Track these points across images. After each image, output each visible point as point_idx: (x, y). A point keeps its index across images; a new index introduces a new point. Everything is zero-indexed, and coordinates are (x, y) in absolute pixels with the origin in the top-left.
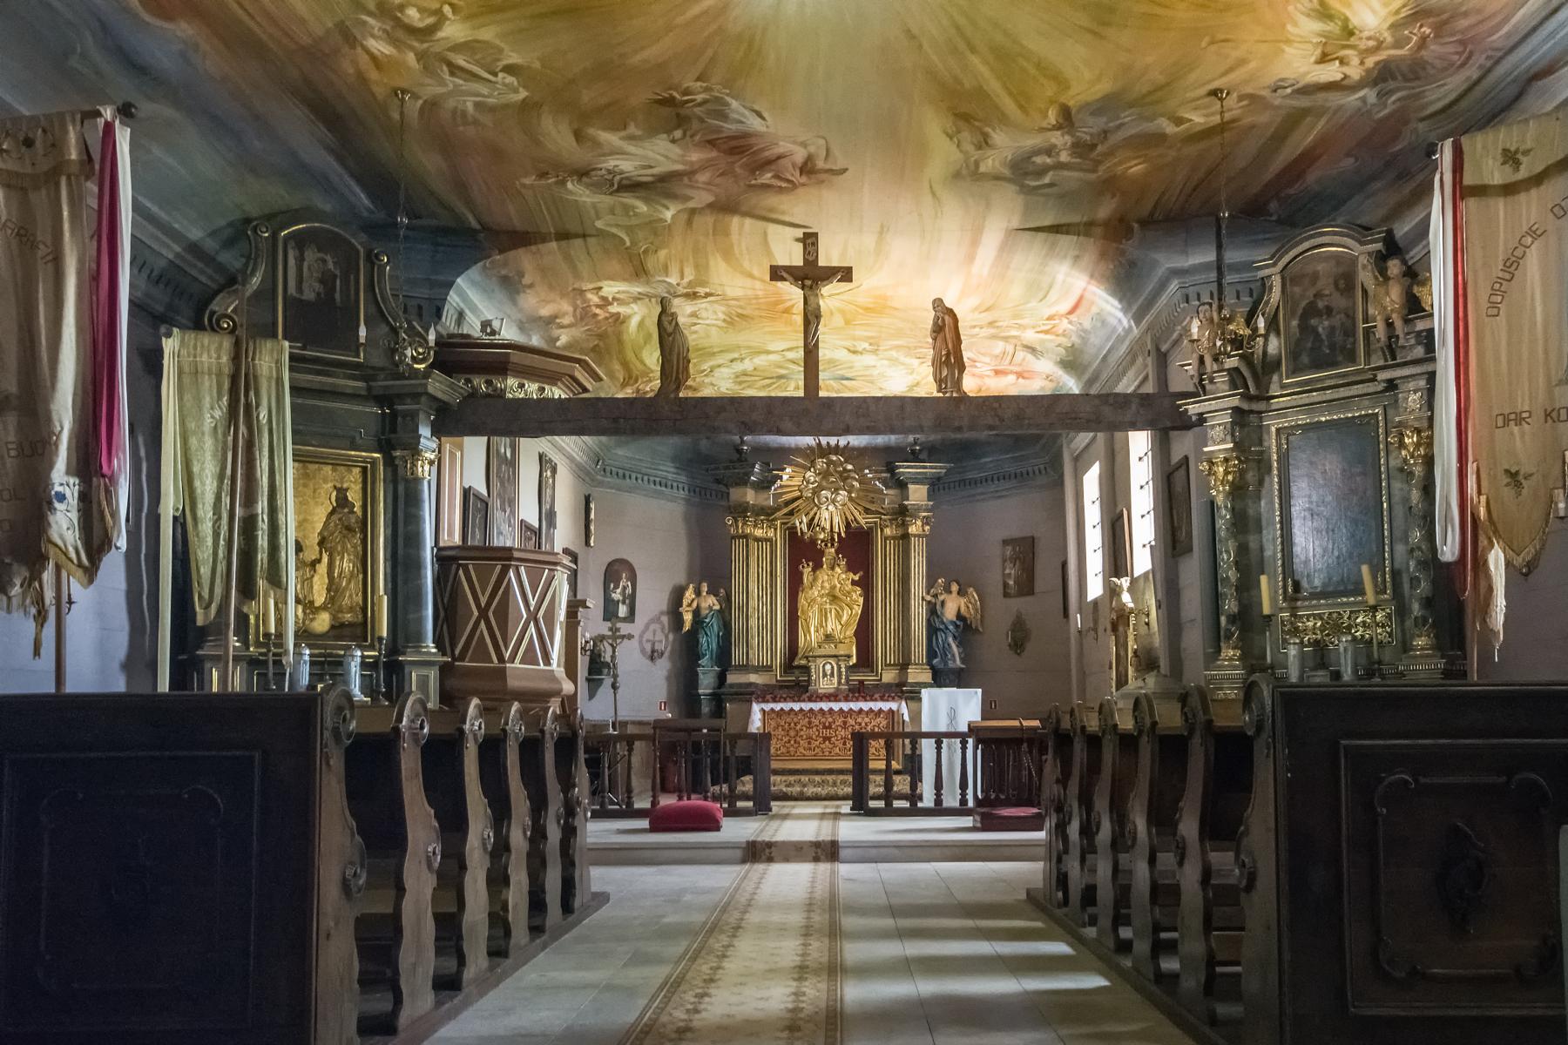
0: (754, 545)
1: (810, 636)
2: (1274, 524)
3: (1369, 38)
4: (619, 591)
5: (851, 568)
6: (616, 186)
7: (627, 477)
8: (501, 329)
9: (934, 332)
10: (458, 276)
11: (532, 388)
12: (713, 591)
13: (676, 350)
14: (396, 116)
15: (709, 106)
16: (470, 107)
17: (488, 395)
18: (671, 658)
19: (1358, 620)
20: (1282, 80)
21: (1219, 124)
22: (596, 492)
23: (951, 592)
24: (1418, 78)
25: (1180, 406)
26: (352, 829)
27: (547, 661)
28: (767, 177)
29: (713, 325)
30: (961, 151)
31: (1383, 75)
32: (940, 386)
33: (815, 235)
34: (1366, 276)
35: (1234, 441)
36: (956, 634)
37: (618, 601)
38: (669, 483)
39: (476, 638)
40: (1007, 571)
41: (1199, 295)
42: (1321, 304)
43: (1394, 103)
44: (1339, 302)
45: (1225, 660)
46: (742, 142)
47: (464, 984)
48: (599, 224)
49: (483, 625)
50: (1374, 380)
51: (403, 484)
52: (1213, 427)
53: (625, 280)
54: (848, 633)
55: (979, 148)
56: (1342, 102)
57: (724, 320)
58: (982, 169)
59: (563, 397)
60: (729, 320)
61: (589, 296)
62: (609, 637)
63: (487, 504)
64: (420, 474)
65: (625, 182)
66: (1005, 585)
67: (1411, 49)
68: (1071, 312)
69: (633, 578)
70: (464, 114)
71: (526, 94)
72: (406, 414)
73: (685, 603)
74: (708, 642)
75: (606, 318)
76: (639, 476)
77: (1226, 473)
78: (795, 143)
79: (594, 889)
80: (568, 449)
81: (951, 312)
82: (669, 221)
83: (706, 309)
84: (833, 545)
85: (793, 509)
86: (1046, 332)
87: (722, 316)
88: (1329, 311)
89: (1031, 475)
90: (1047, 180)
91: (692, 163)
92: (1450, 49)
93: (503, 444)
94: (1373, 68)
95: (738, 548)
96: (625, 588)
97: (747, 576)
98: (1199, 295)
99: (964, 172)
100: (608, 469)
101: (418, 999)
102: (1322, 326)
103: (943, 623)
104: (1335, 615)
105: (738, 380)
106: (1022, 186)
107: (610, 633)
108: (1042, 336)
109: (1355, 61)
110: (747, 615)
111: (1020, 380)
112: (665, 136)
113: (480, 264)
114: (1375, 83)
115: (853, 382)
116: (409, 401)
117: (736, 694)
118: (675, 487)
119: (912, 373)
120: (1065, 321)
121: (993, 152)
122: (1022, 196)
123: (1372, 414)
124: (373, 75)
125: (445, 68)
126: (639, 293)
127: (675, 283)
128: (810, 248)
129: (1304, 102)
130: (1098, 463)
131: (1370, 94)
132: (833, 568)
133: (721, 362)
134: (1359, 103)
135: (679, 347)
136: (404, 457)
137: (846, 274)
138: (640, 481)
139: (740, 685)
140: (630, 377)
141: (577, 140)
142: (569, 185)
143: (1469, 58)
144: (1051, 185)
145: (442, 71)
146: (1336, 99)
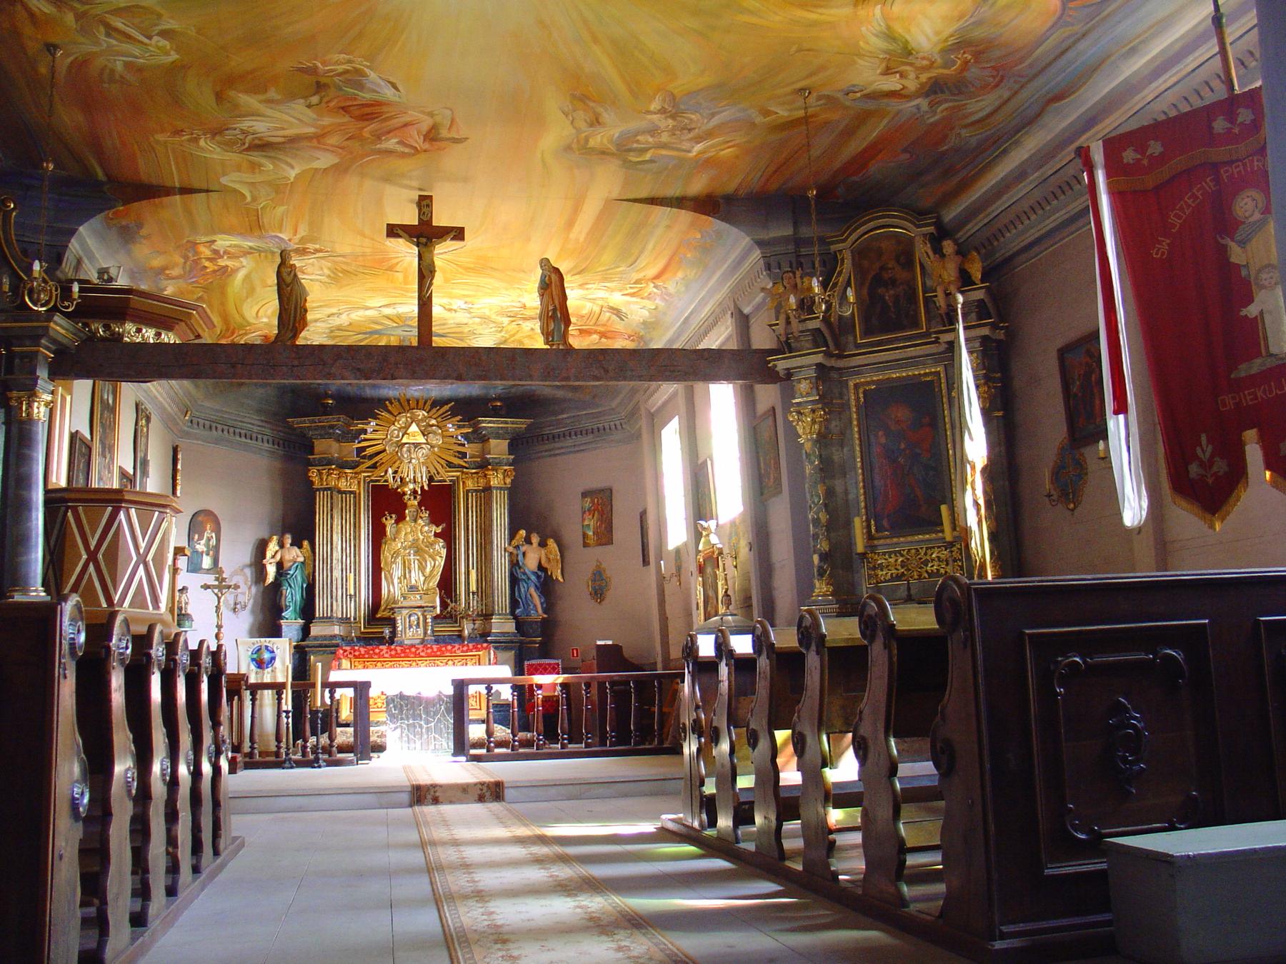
0: (337, 497)
1: (392, 588)
2: (855, 468)
3: (923, 58)
4: (203, 542)
5: (434, 520)
6: (247, 145)
7: (214, 428)
8: (118, 276)
9: (542, 289)
10: (80, 225)
11: (149, 334)
12: (297, 543)
13: (294, 302)
14: (43, 70)
15: (347, 76)
16: (119, 67)
17: (103, 339)
18: (253, 612)
19: (933, 556)
20: (854, 86)
21: (804, 117)
22: (182, 443)
23: (531, 544)
24: (960, 93)
25: (769, 362)
26: (78, 746)
27: (156, 606)
28: (391, 143)
29: (317, 280)
30: (575, 128)
31: (935, 89)
32: (547, 339)
33: (430, 197)
34: (922, 250)
35: (819, 394)
36: (538, 584)
37: (203, 552)
38: (254, 435)
39: (84, 582)
40: (586, 523)
41: (779, 264)
42: (886, 276)
43: (942, 112)
44: (901, 274)
45: (819, 596)
46: (377, 109)
47: (150, 919)
48: (224, 180)
49: (91, 568)
50: (936, 341)
51: (17, 425)
52: (799, 381)
53: (240, 234)
54: (431, 584)
55: (591, 125)
56: (900, 107)
57: (329, 276)
58: (592, 143)
59: (177, 342)
60: (332, 275)
61: (202, 249)
62: (215, 587)
63: (90, 450)
64: (35, 416)
65: (257, 142)
66: (585, 536)
67: (955, 70)
68: (657, 277)
69: (217, 530)
70: (112, 71)
71: (178, 57)
72: (23, 356)
73: (269, 554)
74: (292, 595)
75: (214, 271)
76: (226, 428)
77: (814, 422)
78: (423, 112)
79: (234, 834)
80: (158, 392)
81: (557, 270)
82: (292, 179)
83: (313, 265)
84: (415, 498)
85: (376, 463)
86: (632, 295)
87: (327, 272)
88: (893, 282)
89: (608, 430)
90: (648, 156)
91: (324, 127)
92: (987, 73)
93: (105, 387)
94: (926, 82)
95: (321, 502)
96: (209, 539)
97: (332, 527)
98: (779, 264)
99: (575, 146)
100: (195, 421)
101: (120, 932)
102: (888, 295)
103: (525, 573)
104: (913, 551)
105: (332, 334)
106: (625, 161)
107: (217, 583)
108: (628, 298)
109: (912, 76)
110: (331, 567)
111: (603, 340)
112: (302, 101)
113: (103, 215)
114: (927, 95)
115: (443, 338)
116: (28, 343)
117: (320, 646)
118: (260, 439)
119: (501, 331)
120: (652, 285)
121: (602, 130)
122: (624, 170)
123: (935, 372)
124: (28, 30)
125: (102, 29)
126: (251, 248)
127: (287, 239)
128: (425, 210)
129: (871, 105)
130: (677, 417)
131: (923, 103)
132: (415, 521)
133: (318, 316)
134: (915, 110)
135: (297, 296)
136: (20, 398)
137: (458, 234)
138: (225, 432)
139: (324, 638)
140: (227, 330)
141: (217, 101)
142: (202, 143)
143: (1001, 81)
144: (651, 161)
145: (98, 32)
146: (895, 105)
